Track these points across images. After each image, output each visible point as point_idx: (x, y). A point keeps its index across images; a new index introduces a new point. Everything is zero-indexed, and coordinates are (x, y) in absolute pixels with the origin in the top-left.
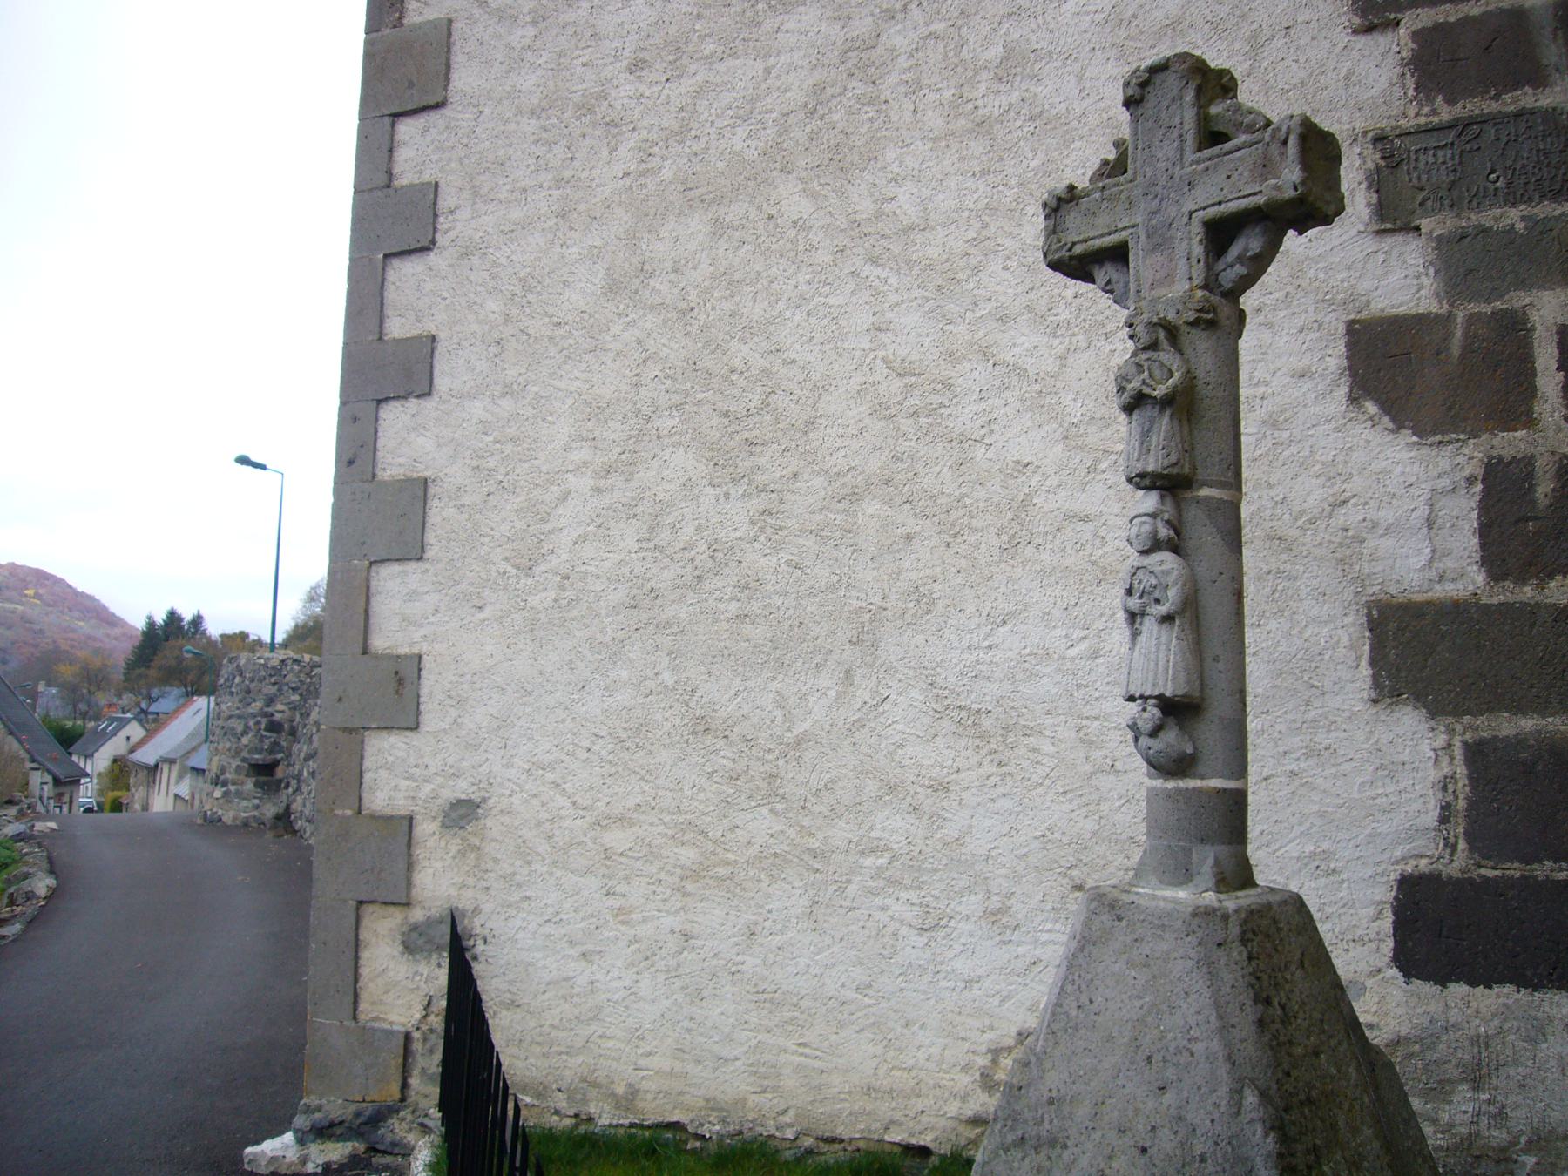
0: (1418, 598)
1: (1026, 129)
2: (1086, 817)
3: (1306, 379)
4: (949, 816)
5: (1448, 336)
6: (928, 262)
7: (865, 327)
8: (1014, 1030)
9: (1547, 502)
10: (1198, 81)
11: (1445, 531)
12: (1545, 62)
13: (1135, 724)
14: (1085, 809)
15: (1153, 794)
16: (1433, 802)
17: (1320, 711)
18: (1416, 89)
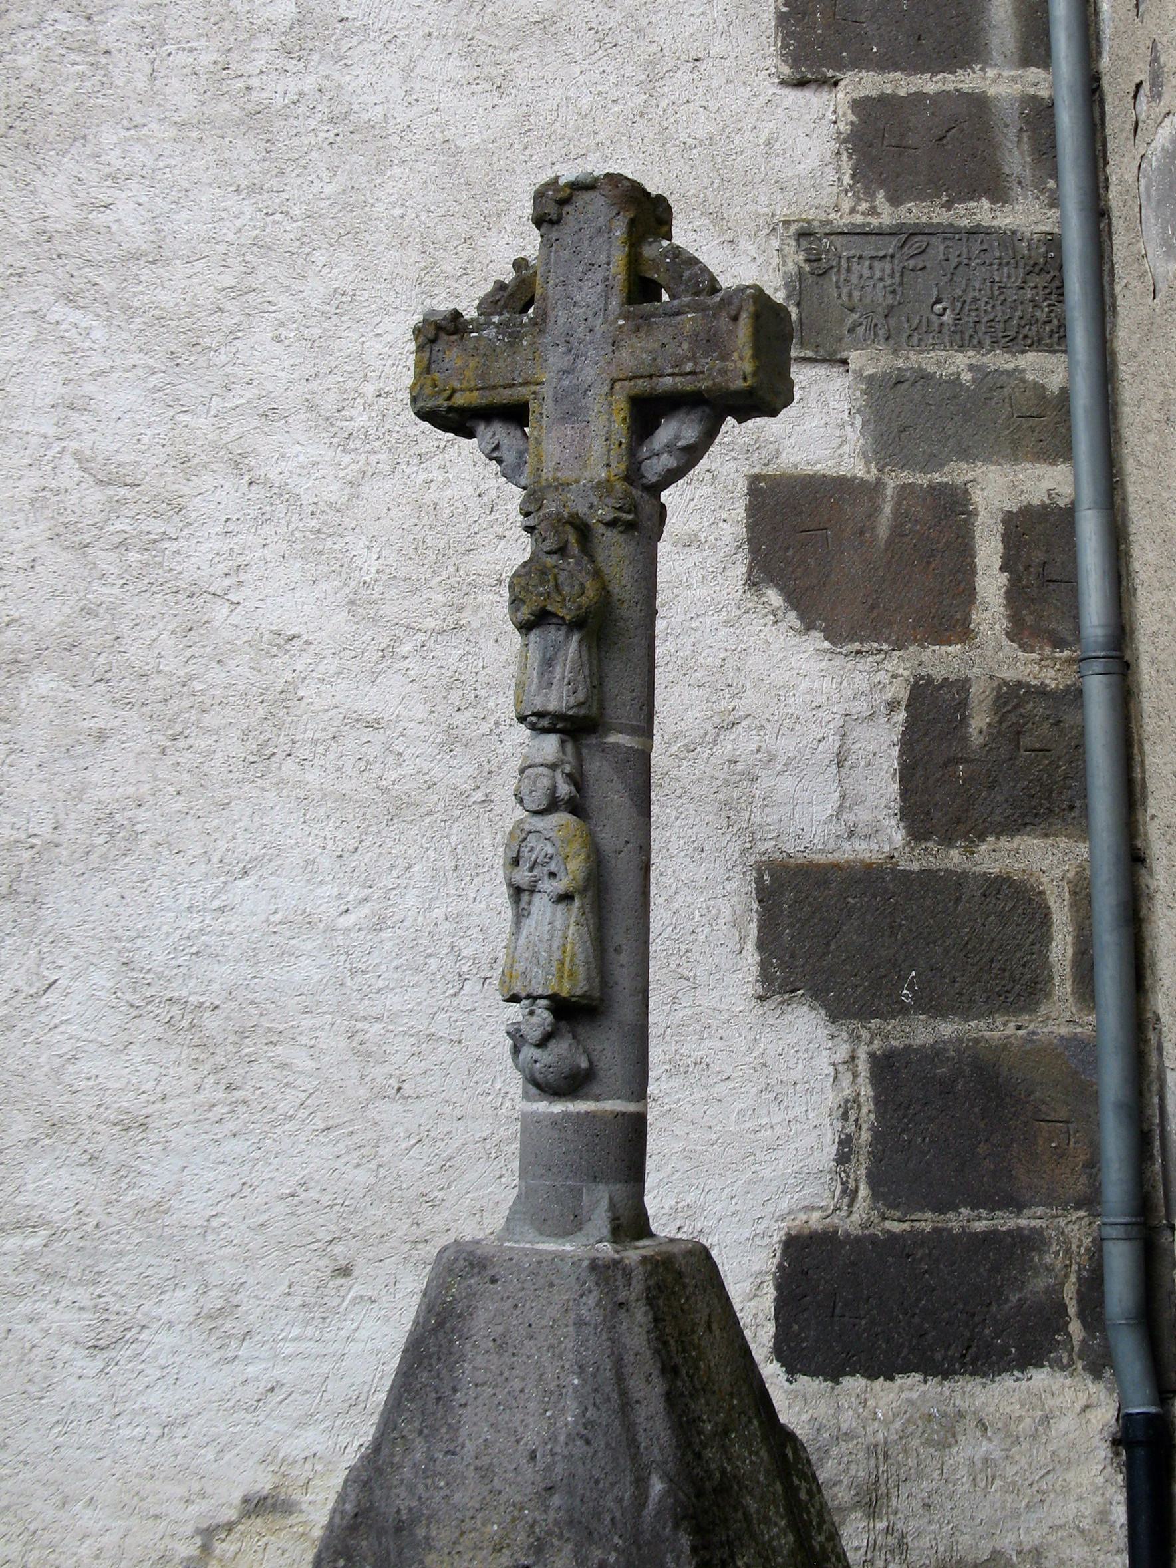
0: (822, 859)
1: (322, 135)
2: (358, 1165)
3: (692, 549)
4: (147, 1167)
5: (877, 509)
6: (157, 312)
7: (49, 401)
8: (237, 1496)
9: (981, 740)
10: (631, 214)
11: (859, 771)
12: (1007, 170)
13: (518, 1030)
14: (356, 1154)
15: (529, 1124)
16: (830, 1135)
17: (690, 1012)
18: (853, 176)
